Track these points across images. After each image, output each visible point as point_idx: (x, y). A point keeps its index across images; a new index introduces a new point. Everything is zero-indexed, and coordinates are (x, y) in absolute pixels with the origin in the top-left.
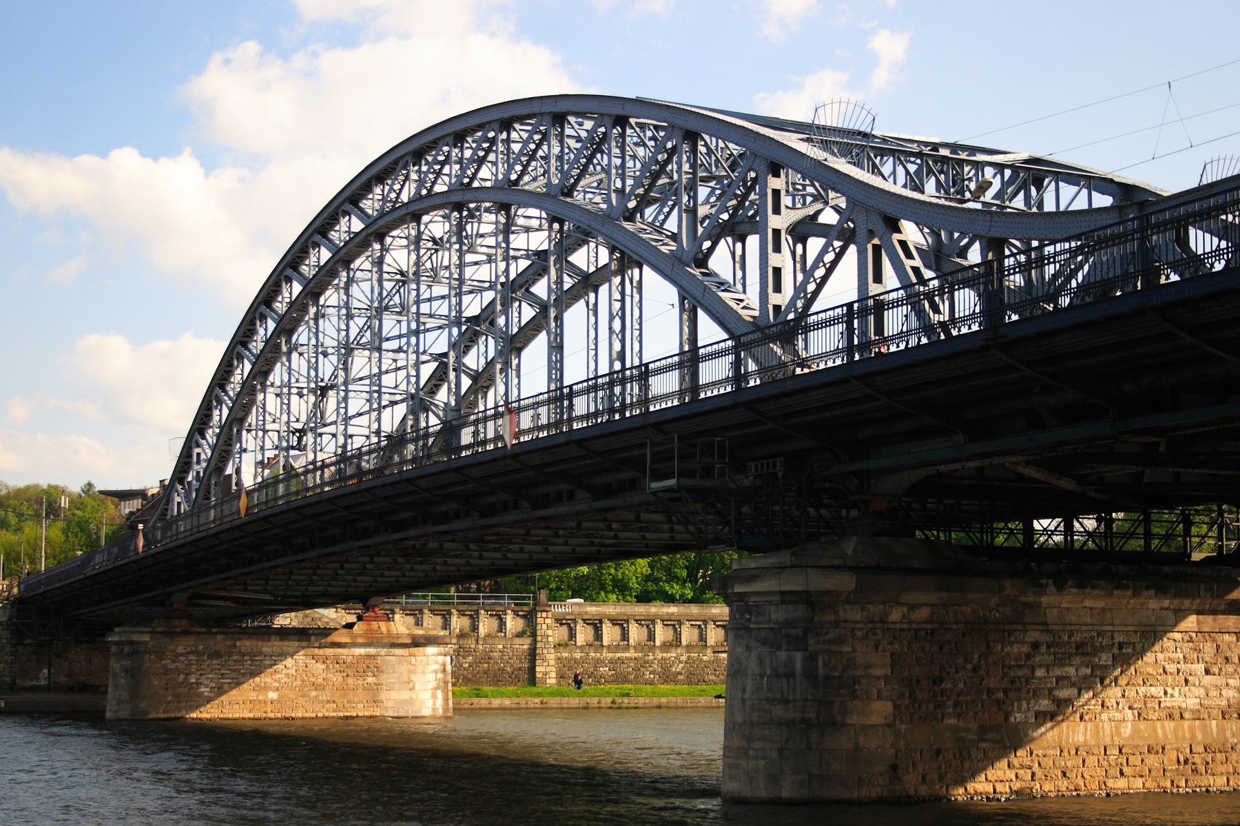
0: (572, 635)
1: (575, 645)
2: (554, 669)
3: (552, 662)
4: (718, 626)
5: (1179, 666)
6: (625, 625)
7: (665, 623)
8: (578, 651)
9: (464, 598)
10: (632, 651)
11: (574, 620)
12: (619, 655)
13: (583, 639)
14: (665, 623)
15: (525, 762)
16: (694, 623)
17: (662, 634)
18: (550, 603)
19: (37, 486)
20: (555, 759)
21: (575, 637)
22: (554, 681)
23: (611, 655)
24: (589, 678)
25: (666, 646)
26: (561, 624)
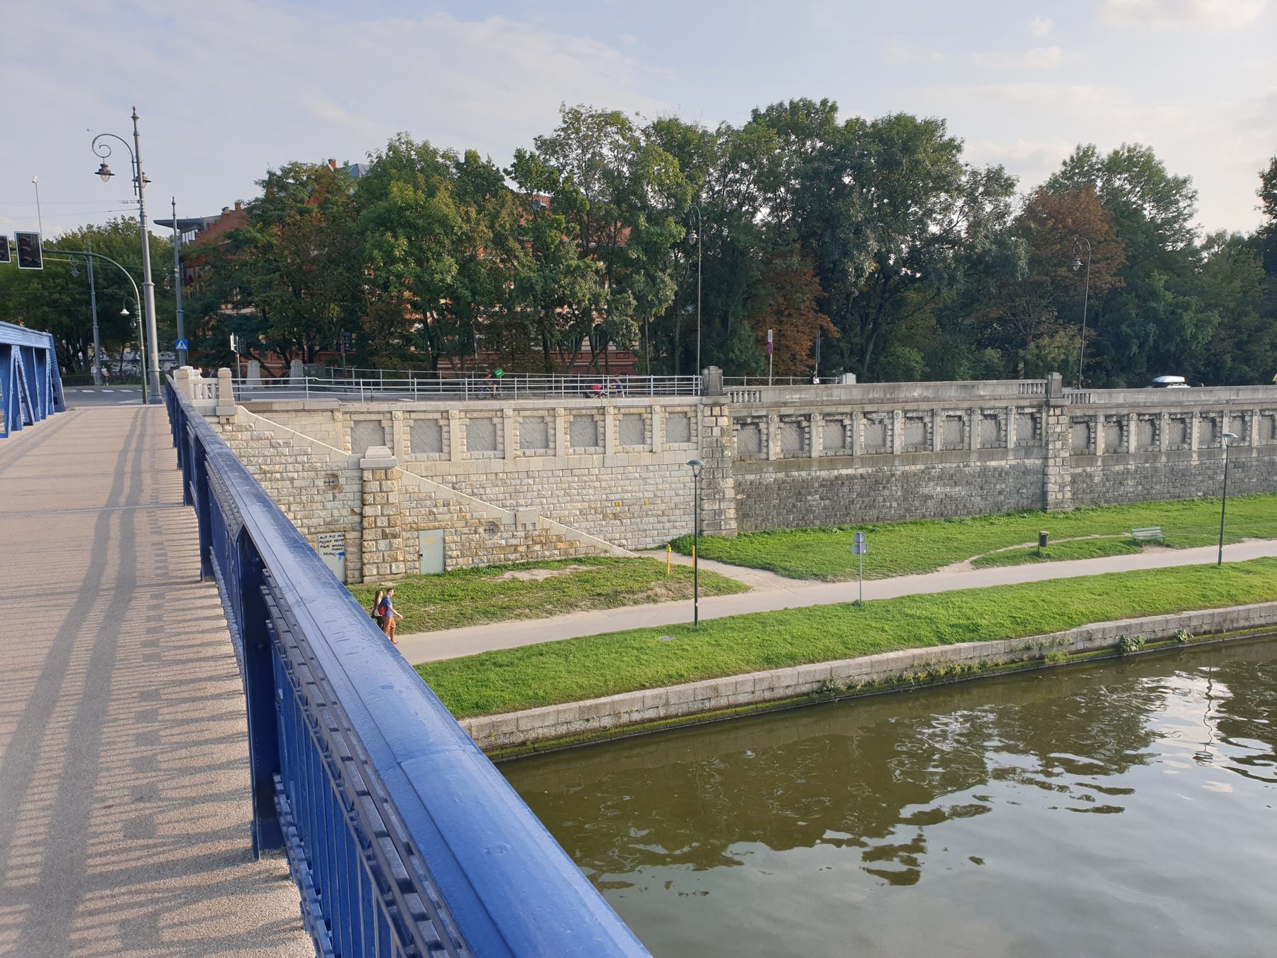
0: (762, 444)
1: (768, 459)
2: (733, 505)
3: (730, 493)
4: (986, 416)
5: (376, 453)
6: (495, 420)
7: (827, 418)
8: (771, 469)
9: (388, 384)
10: (1011, 456)
11: (1158, 416)
12: (836, 473)
13: (778, 449)
14: (909, 415)
15: (1000, 689)
16: (951, 413)
17: (981, 431)
18: (725, 389)
19: (912, 119)
20: (1181, 660)
21: (1190, 438)
22: (734, 525)
23: (824, 474)
24: (788, 513)
25: (910, 455)
26: (744, 425)
